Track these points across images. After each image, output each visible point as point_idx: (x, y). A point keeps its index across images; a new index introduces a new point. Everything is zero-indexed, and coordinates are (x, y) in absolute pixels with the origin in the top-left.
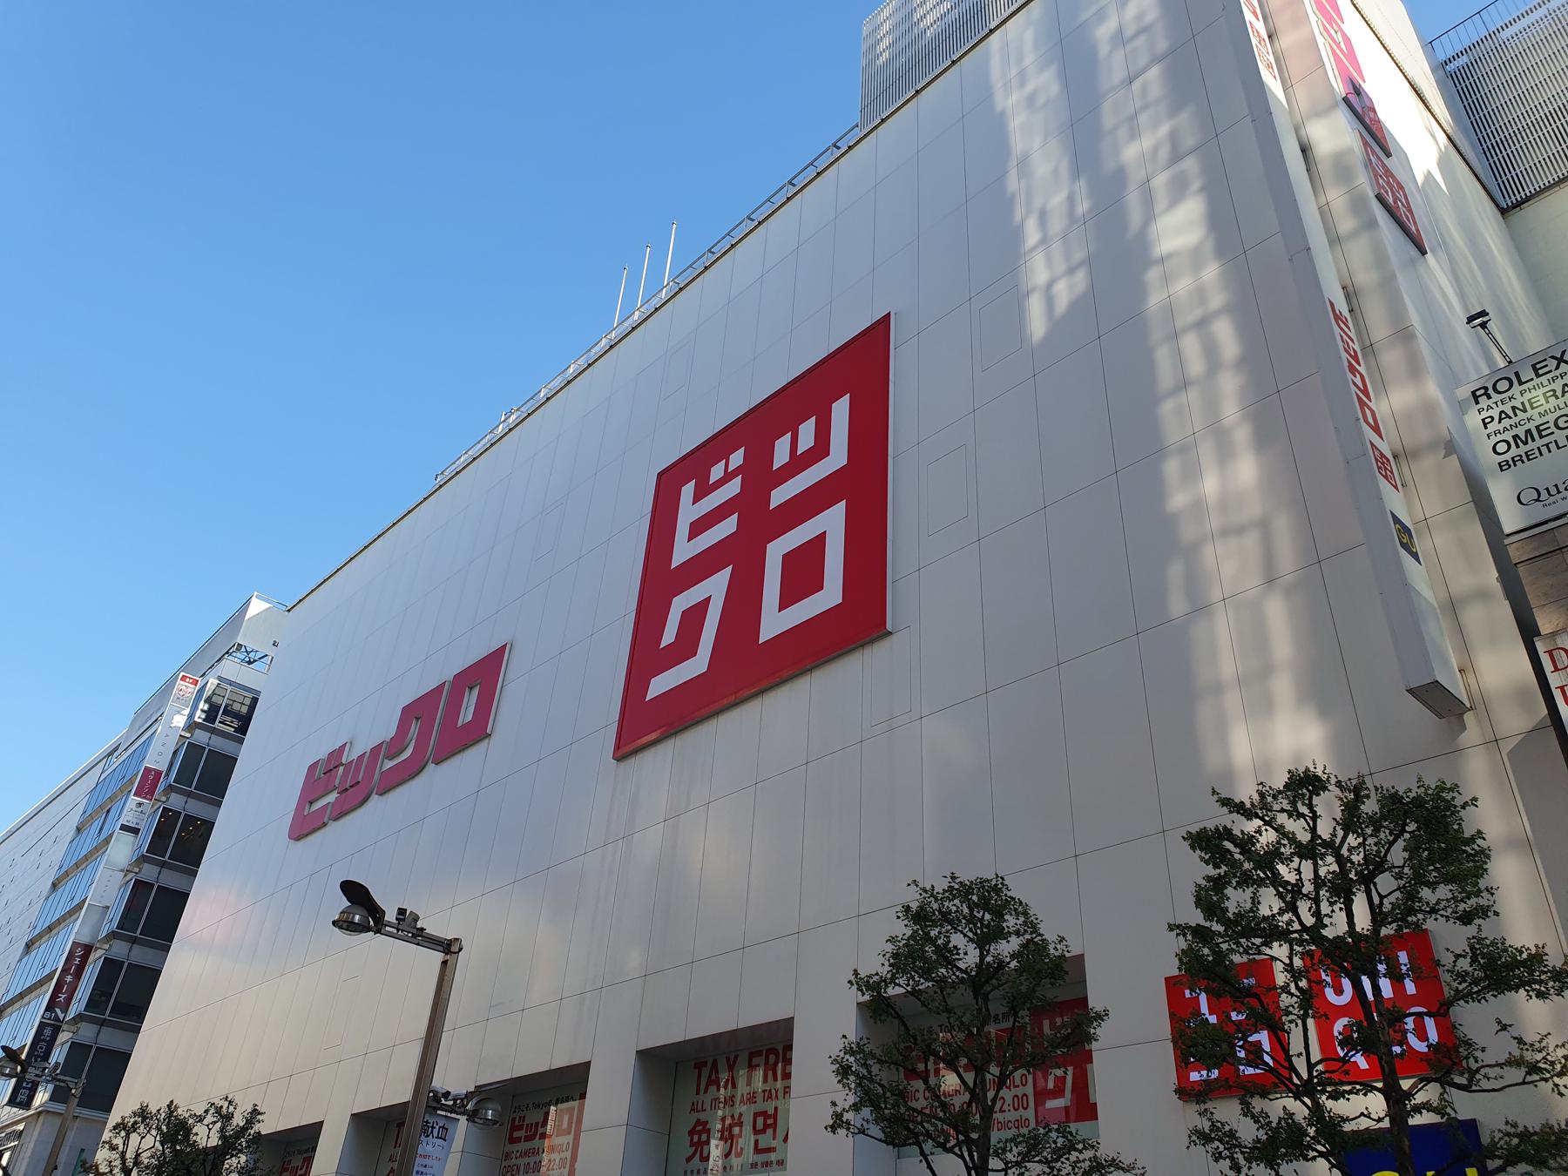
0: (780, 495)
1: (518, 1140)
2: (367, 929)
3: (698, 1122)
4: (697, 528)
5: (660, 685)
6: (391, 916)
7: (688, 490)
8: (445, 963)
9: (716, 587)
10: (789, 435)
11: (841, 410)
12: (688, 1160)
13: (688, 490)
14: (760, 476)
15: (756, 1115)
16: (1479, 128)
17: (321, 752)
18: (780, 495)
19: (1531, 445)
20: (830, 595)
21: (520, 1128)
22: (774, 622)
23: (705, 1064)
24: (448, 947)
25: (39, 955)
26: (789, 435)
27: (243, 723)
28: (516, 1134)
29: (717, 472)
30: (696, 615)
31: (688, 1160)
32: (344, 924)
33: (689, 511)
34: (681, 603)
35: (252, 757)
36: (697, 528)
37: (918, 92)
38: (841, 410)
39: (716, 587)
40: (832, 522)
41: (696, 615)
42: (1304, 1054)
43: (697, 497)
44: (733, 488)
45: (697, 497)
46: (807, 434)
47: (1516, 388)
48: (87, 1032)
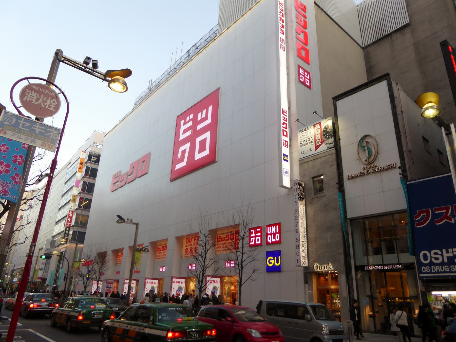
0: (199, 127)
1: (158, 251)
2: (122, 222)
3: (187, 248)
4: (185, 131)
5: (178, 166)
6: (126, 220)
7: (182, 122)
8: (137, 227)
9: (187, 146)
10: (201, 113)
11: (210, 108)
12: (185, 254)
13: (182, 122)
14: (196, 122)
15: (195, 247)
16: (379, 8)
17: (115, 172)
18: (199, 127)
19: (305, 143)
20: (206, 153)
21: (158, 249)
22: (198, 156)
23: (187, 239)
24: (137, 224)
25: (62, 212)
26: (201, 113)
27: (97, 161)
28: (158, 250)
29: (188, 119)
30: (184, 152)
31: (185, 254)
32: (118, 222)
33: (183, 128)
34: (182, 149)
35: (102, 168)
36: (185, 131)
37: (228, 28)
38: (210, 108)
39: (187, 146)
40: (207, 135)
41: (184, 152)
42: (134, 271)
43: (184, 124)
44: (190, 124)
45: (184, 124)
46: (204, 112)
47: (305, 131)
48: (76, 229)
